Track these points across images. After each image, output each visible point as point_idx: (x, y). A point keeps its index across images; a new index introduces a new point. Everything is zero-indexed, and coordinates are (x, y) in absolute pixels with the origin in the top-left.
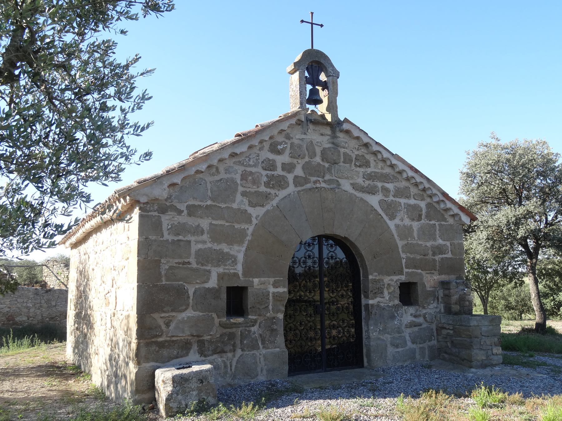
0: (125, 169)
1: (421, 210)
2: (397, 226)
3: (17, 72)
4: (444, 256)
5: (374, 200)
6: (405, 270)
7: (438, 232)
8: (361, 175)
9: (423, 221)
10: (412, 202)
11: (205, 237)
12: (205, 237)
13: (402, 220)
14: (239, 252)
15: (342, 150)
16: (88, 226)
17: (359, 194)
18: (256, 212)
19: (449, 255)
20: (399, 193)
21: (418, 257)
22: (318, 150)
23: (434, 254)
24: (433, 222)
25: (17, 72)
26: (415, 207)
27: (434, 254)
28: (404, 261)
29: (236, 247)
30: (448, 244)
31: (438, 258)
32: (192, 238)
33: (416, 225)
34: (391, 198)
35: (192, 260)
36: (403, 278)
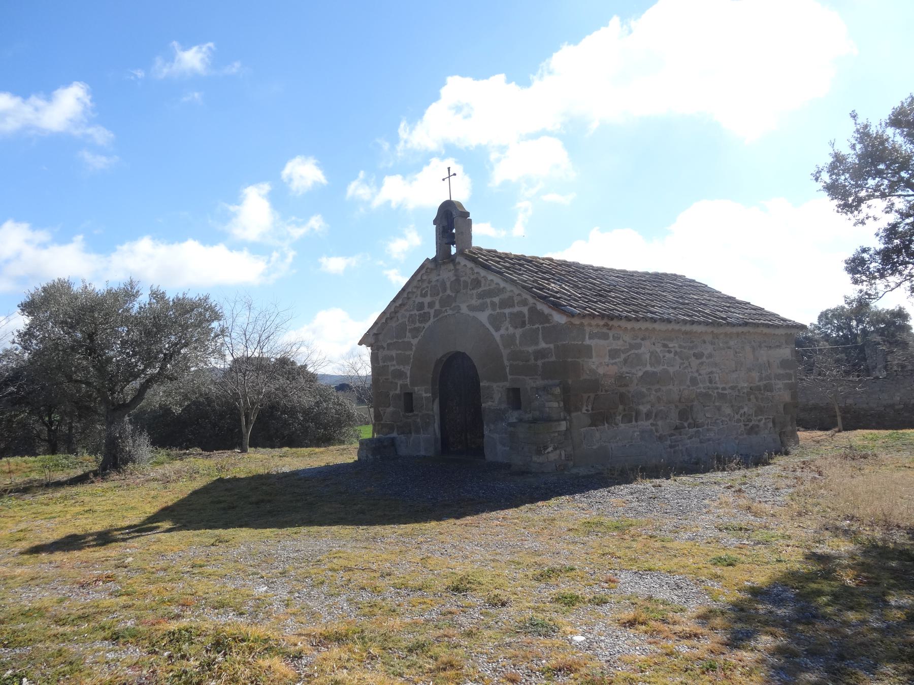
0: (360, 343)
1: (524, 316)
2: (502, 336)
3: (378, 457)
4: (546, 360)
5: (483, 317)
6: (509, 377)
7: (540, 336)
8: (475, 296)
9: (527, 327)
10: (516, 309)
11: (395, 362)
12: (395, 362)
13: (507, 329)
14: (407, 369)
15: (462, 279)
16: (647, 291)
17: (472, 314)
18: (415, 342)
19: (553, 359)
20: (504, 304)
21: (521, 363)
22: (448, 285)
23: (536, 359)
24: (537, 326)
25: (378, 457)
26: (520, 314)
27: (536, 359)
28: (508, 370)
29: (407, 367)
30: (552, 346)
31: (540, 363)
32: (389, 363)
33: (519, 332)
34: (498, 311)
35: (390, 377)
36: (507, 384)
